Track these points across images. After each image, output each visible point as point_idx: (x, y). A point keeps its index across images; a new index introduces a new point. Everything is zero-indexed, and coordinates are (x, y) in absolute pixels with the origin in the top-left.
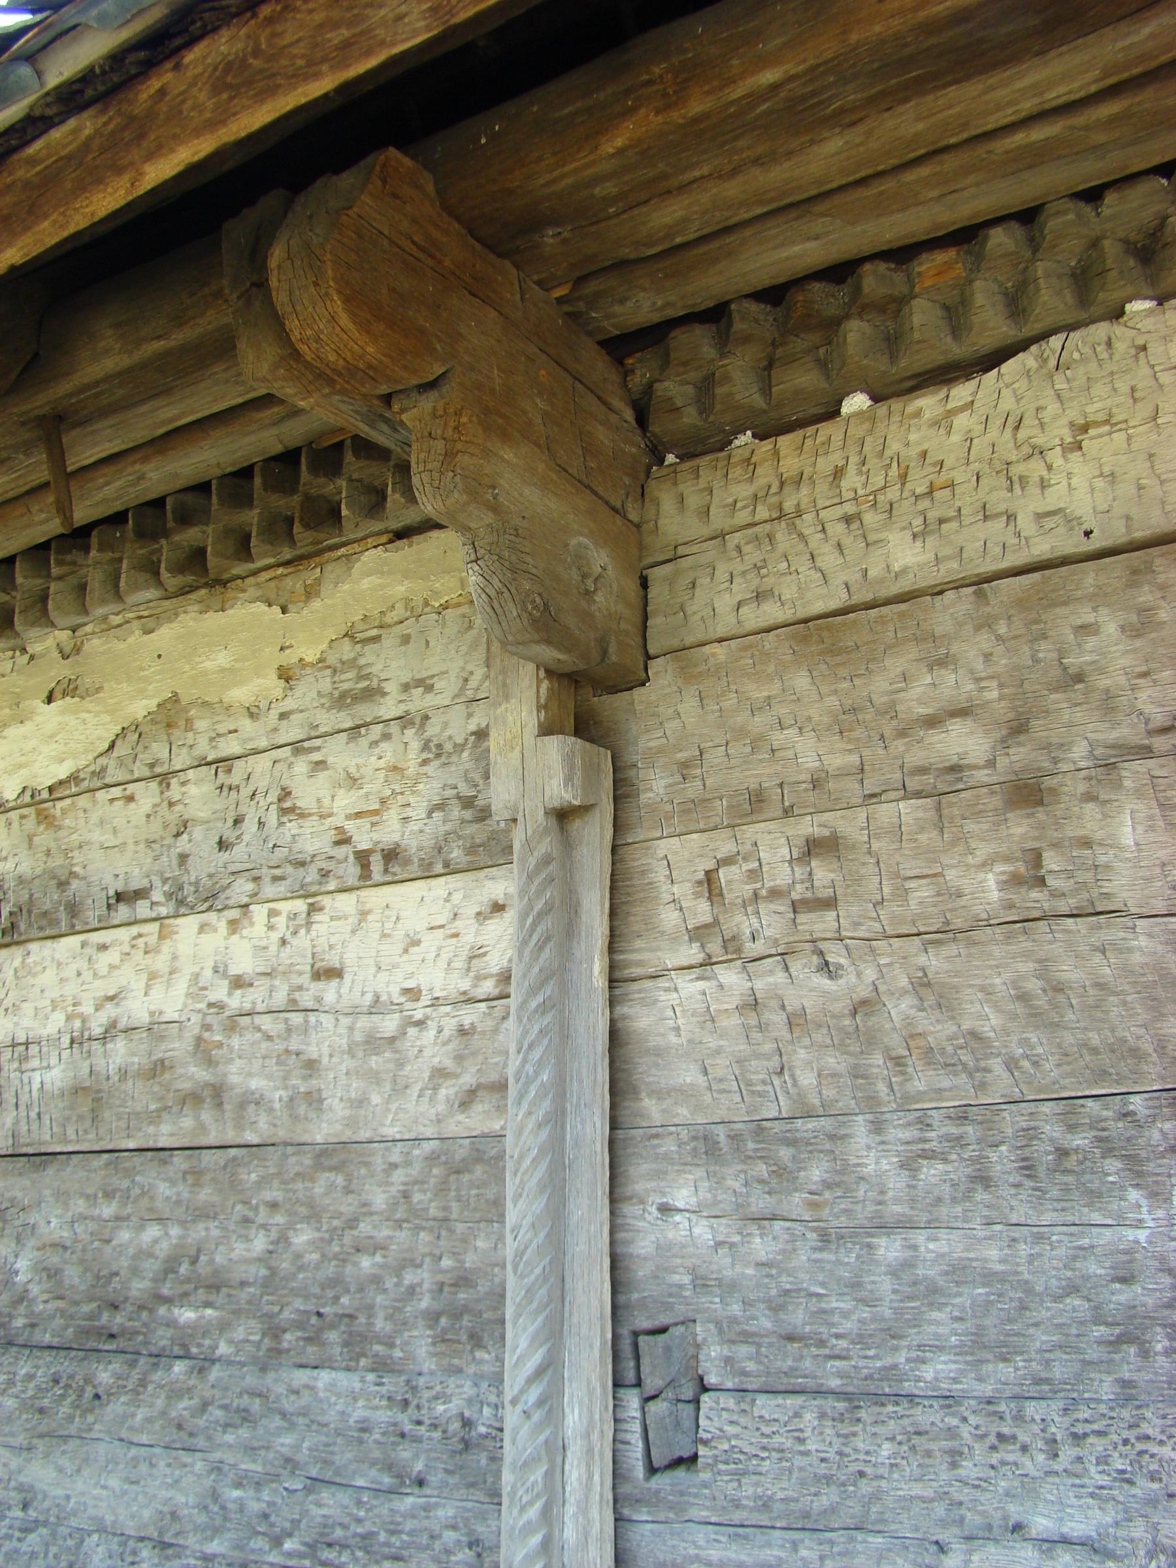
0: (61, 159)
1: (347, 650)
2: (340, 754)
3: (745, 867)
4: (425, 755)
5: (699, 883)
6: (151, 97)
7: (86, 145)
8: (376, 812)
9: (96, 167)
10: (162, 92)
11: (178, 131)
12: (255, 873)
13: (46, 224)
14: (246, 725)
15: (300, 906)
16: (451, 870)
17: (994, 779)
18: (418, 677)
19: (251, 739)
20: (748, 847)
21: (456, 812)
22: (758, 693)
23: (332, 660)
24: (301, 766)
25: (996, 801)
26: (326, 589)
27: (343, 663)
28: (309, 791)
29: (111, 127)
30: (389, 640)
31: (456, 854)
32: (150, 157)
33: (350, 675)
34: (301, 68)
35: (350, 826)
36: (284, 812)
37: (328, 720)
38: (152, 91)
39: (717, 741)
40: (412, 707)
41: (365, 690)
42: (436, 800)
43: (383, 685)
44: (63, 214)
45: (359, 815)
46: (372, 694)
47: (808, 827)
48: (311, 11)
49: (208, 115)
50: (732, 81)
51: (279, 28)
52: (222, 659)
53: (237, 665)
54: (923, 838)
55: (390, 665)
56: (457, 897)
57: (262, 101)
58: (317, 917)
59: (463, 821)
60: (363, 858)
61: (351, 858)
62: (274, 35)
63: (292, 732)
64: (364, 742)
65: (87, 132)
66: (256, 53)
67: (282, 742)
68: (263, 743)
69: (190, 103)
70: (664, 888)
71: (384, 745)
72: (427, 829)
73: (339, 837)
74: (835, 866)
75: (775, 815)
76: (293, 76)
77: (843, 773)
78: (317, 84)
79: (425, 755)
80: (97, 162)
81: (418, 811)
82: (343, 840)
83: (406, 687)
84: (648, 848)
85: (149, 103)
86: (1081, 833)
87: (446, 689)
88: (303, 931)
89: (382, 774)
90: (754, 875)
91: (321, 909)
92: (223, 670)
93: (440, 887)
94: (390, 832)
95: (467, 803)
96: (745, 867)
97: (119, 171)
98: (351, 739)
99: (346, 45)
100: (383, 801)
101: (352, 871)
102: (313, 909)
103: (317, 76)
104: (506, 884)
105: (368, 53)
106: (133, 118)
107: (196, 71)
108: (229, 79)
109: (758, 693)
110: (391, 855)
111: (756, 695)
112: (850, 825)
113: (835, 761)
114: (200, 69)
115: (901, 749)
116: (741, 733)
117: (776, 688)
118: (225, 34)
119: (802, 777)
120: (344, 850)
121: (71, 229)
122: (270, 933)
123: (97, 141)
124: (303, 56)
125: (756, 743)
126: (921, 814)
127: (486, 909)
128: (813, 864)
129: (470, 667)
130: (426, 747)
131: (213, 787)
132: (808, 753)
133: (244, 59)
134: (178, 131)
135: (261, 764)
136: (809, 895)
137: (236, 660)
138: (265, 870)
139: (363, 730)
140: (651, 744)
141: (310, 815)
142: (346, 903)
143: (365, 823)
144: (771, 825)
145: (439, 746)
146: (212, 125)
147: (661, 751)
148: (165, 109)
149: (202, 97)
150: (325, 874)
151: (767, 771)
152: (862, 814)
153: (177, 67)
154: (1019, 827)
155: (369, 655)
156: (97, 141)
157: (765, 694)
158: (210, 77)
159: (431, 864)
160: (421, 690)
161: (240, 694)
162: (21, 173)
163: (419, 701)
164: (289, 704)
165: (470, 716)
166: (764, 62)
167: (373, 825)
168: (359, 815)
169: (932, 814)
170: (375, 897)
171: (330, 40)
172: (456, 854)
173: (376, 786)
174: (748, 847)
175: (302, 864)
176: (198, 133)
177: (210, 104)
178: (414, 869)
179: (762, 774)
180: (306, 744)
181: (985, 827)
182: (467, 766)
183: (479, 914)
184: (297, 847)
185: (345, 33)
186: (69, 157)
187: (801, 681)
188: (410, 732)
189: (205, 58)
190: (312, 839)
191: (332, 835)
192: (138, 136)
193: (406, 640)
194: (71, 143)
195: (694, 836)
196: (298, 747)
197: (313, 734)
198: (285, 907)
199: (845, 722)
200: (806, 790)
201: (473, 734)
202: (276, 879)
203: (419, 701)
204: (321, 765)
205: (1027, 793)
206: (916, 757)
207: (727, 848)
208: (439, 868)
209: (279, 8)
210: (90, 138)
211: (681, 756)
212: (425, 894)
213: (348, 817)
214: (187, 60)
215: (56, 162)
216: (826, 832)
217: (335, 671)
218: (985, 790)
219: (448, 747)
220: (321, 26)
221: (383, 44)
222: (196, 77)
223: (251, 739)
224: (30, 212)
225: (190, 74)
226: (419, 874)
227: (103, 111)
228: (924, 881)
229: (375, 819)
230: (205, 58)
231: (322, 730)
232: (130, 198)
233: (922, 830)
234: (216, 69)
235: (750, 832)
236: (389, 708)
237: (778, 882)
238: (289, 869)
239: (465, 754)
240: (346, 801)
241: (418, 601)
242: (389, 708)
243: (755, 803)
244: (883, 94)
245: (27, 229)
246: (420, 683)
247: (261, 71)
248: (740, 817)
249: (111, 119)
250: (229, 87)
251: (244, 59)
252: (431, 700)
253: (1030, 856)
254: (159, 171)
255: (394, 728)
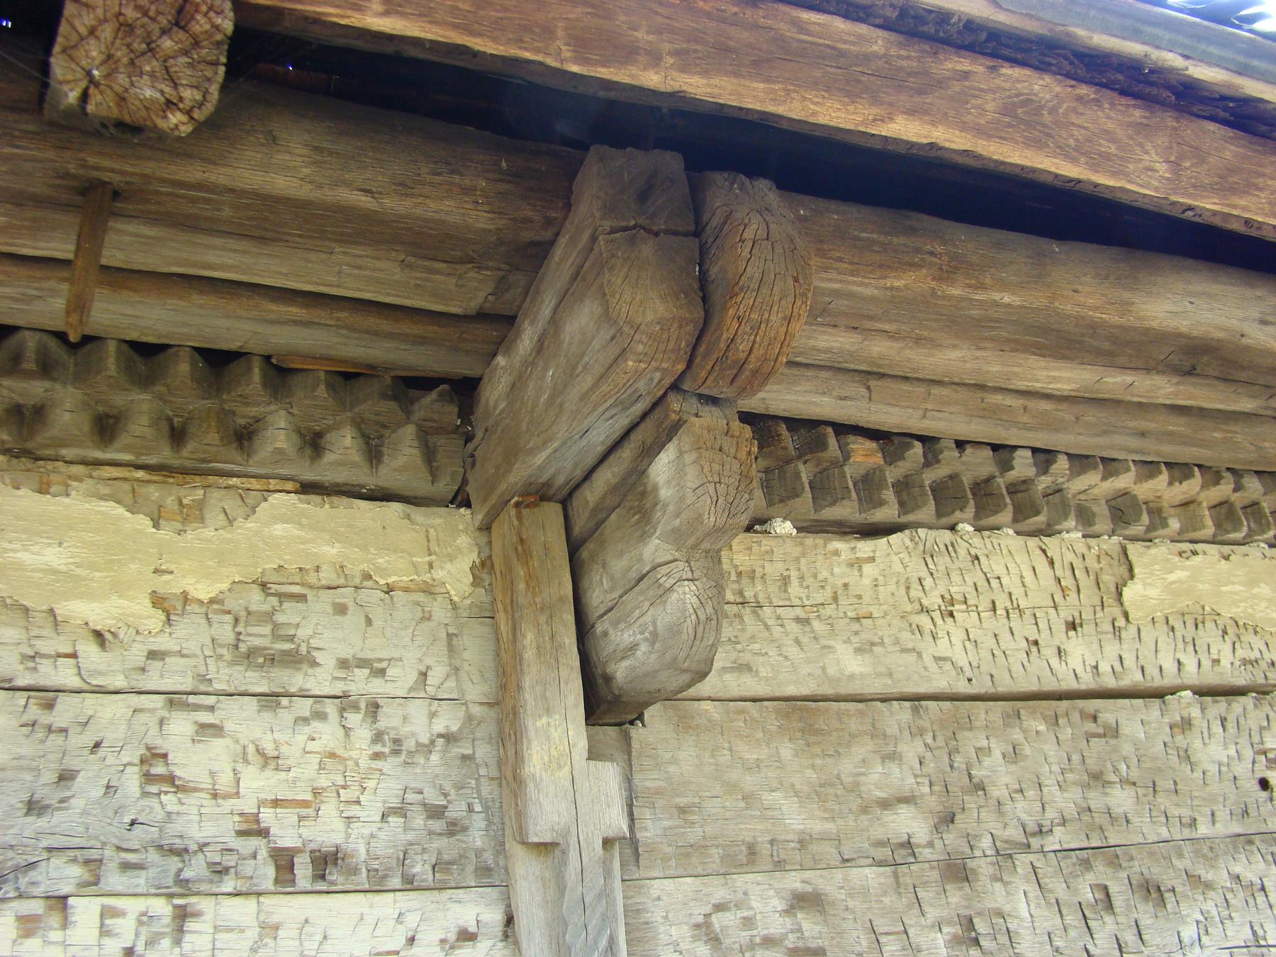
0: (833, 48)
1: (256, 600)
2: (244, 721)
3: (739, 914)
4: (378, 748)
5: (697, 926)
6: (955, 71)
7: (867, 58)
8: (305, 804)
9: (858, 81)
10: (966, 75)
11: (952, 113)
12: (95, 854)
13: (762, 86)
14: (89, 650)
15: (161, 907)
16: (410, 884)
17: (935, 857)
18: (360, 655)
19: (100, 673)
20: (740, 895)
21: (419, 821)
22: (750, 754)
23: (233, 603)
24: (181, 725)
25: (935, 875)
26: (214, 516)
27: (249, 613)
28: (191, 761)
29: (905, 63)
30: (321, 603)
31: (420, 868)
32: (911, 112)
33: (267, 630)
34: (1069, 146)
35: (267, 816)
36: (148, 778)
37: (225, 676)
38: (959, 67)
39: (715, 793)
40: (353, 688)
41: (285, 653)
42: (395, 802)
43: (315, 653)
44: (788, 92)
45: (276, 803)
46: (296, 659)
47: (794, 881)
48: (1109, 118)
49: (982, 122)
50: (981, 287)
51: (1081, 109)
52: (53, 557)
53: (79, 571)
54: (886, 900)
55: (328, 635)
56: (412, 920)
57: (1027, 146)
58: (190, 925)
59: (431, 833)
60: (284, 862)
61: (263, 853)
62: (1075, 110)
63: (176, 677)
64: (286, 717)
65: (875, 48)
66: (1053, 111)
67: (150, 687)
68: (119, 682)
69: (979, 101)
70: (662, 929)
71: (316, 725)
72: (382, 835)
73: (244, 827)
74: (820, 918)
75: (766, 868)
76: (1060, 147)
77: (824, 837)
78: (1069, 166)
79: (378, 748)
80: (864, 78)
81: (371, 810)
82: (254, 829)
83: (344, 664)
84: (641, 887)
85: (948, 74)
86: (994, 905)
87: (401, 678)
88: (166, 942)
89: (315, 759)
90: (748, 922)
91: (197, 914)
92: (54, 572)
93: (386, 905)
94: (327, 830)
95: (435, 812)
96: (739, 914)
97: (875, 101)
98: (263, 708)
99: (1106, 157)
100: (316, 792)
101: (267, 873)
102: (183, 915)
103: (1074, 161)
104: (477, 910)
105: (1114, 174)
106: (926, 73)
107: (1003, 84)
108: (1020, 111)
109: (750, 754)
110: (327, 862)
111: (747, 756)
112: (830, 883)
113: (817, 827)
114: (1007, 86)
115: (866, 823)
116: (732, 788)
117: (764, 753)
118: (1048, 79)
119: (790, 837)
120: (254, 842)
121: (780, 110)
122: (106, 941)
123: (880, 63)
124: (1077, 140)
125: (748, 798)
126: (883, 880)
127: (452, 937)
128: (799, 916)
129: (429, 661)
130: (378, 737)
131: (15, 723)
132: (796, 819)
133: (1042, 107)
134: (952, 113)
135: (112, 710)
136: (800, 944)
137: (78, 565)
138: (109, 852)
139: (285, 701)
140: (648, 784)
141: (195, 790)
142: (243, 911)
143: (290, 815)
144: (759, 877)
145: (397, 741)
146: (979, 131)
147: (658, 792)
148: (957, 89)
149: (990, 106)
150: (220, 871)
151: (759, 827)
152: (838, 875)
153: (993, 69)
154: (955, 896)
155: (288, 614)
156: (880, 63)
157: (755, 756)
158: (1010, 97)
159: (385, 877)
160: (367, 671)
161: (96, 612)
162: (783, 27)
163: (360, 683)
164: (163, 643)
165: (433, 715)
166: (1003, 286)
167: (301, 818)
168: (276, 803)
169: (891, 880)
170: (287, 909)
171: (1100, 145)
172: (420, 868)
173: (306, 771)
174: (740, 895)
175: (181, 853)
176: (963, 127)
177: (990, 116)
178: (362, 879)
179: (752, 829)
180: (192, 699)
181: (931, 895)
182: (438, 771)
183: (443, 941)
184: (177, 827)
185: (1113, 150)
186: (842, 54)
187: (786, 751)
188: (354, 719)
189: (1018, 81)
190: (204, 823)
191: (233, 823)
192: (918, 92)
193: (341, 610)
194: (845, 42)
195: (689, 880)
196: (175, 700)
197: (202, 688)
198: (133, 906)
199: (819, 794)
200: (793, 849)
201: (441, 736)
202: (126, 866)
203: (360, 683)
204: (215, 730)
205: (957, 871)
206: (878, 833)
207: (720, 894)
208: (396, 882)
209: (1093, 96)
210: (876, 56)
211: (682, 801)
212: (366, 911)
213: (261, 803)
214: (1004, 71)
215: (828, 46)
216: (809, 889)
217: (237, 620)
218: (927, 865)
219: (410, 744)
220: (1107, 132)
221: (1127, 175)
222: (999, 87)
223: (100, 673)
224: (756, 63)
225: (997, 81)
226: (367, 887)
227: (901, 46)
228: (891, 937)
229: (304, 812)
230: (1018, 81)
231: (218, 686)
232: (862, 129)
233: (885, 893)
234: (1018, 95)
235: (743, 881)
236: (321, 680)
237: (772, 931)
238: (153, 856)
239: (435, 758)
240: (257, 784)
241: (355, 570)
242: (321, 680)
243: (748, 857)
244: (1016, 341)
245: (736, 75)
246: (363, 663)
247: (1045, 126)
248: (735, 867)
249: (908, 58)
250: (1016, 117)
251: (1042, 107)
252: (377, 687)
253: (964, 922)
254: (907, 129)
255: (331, 708)
